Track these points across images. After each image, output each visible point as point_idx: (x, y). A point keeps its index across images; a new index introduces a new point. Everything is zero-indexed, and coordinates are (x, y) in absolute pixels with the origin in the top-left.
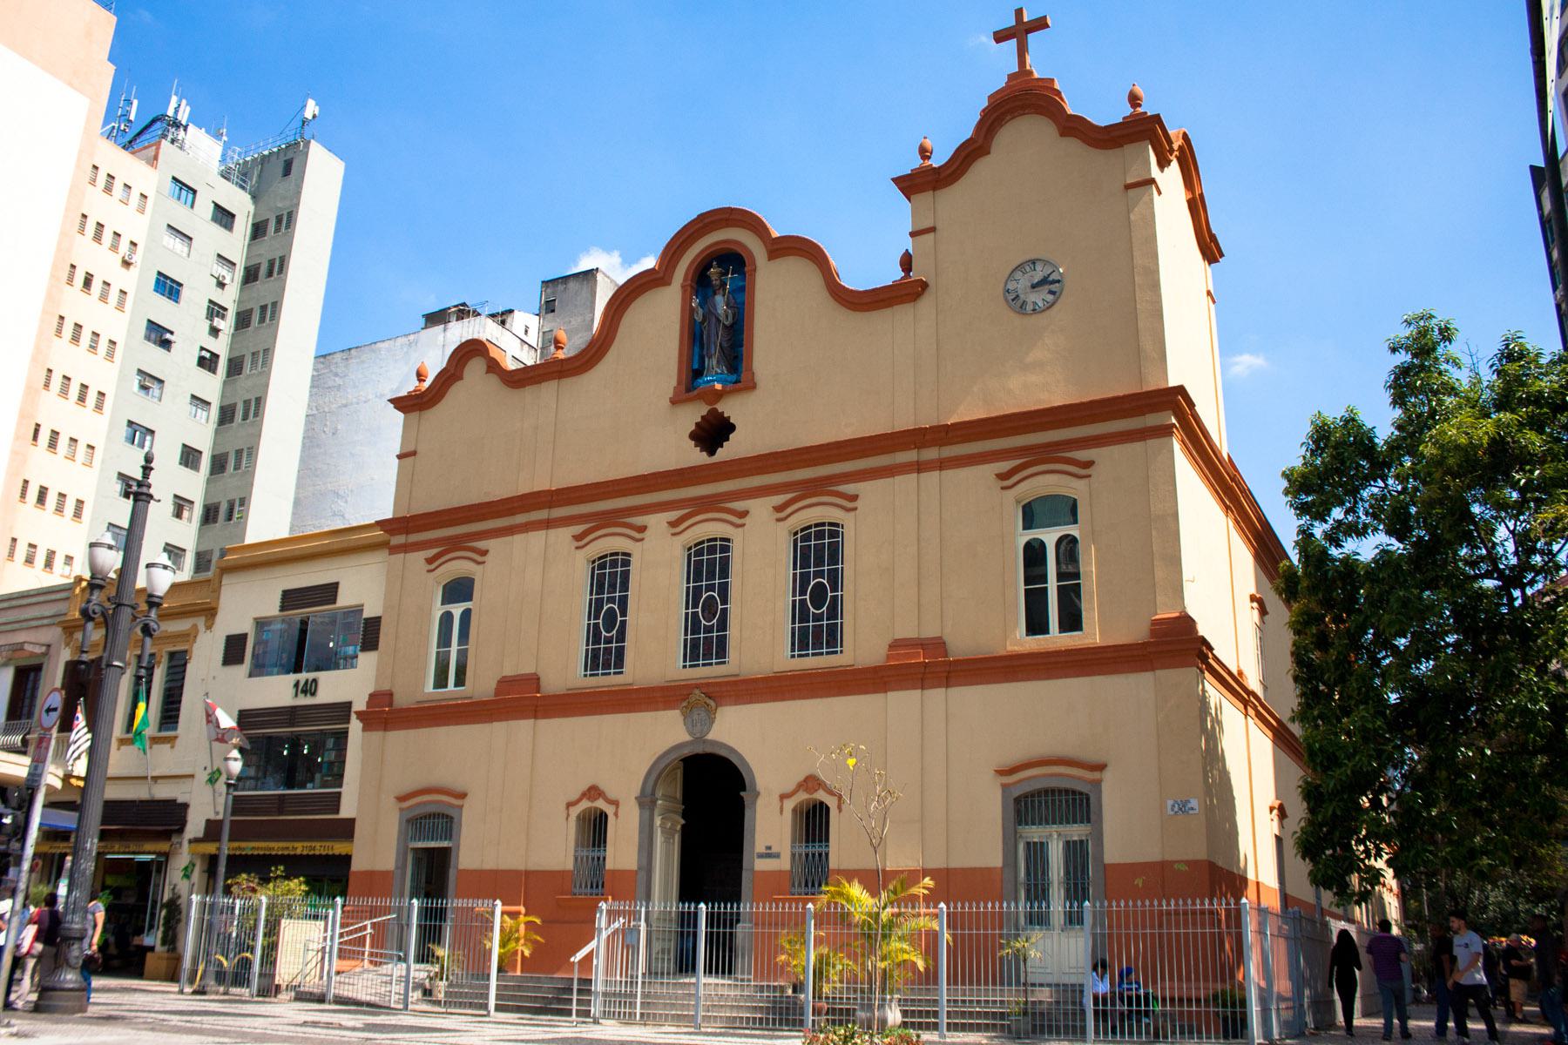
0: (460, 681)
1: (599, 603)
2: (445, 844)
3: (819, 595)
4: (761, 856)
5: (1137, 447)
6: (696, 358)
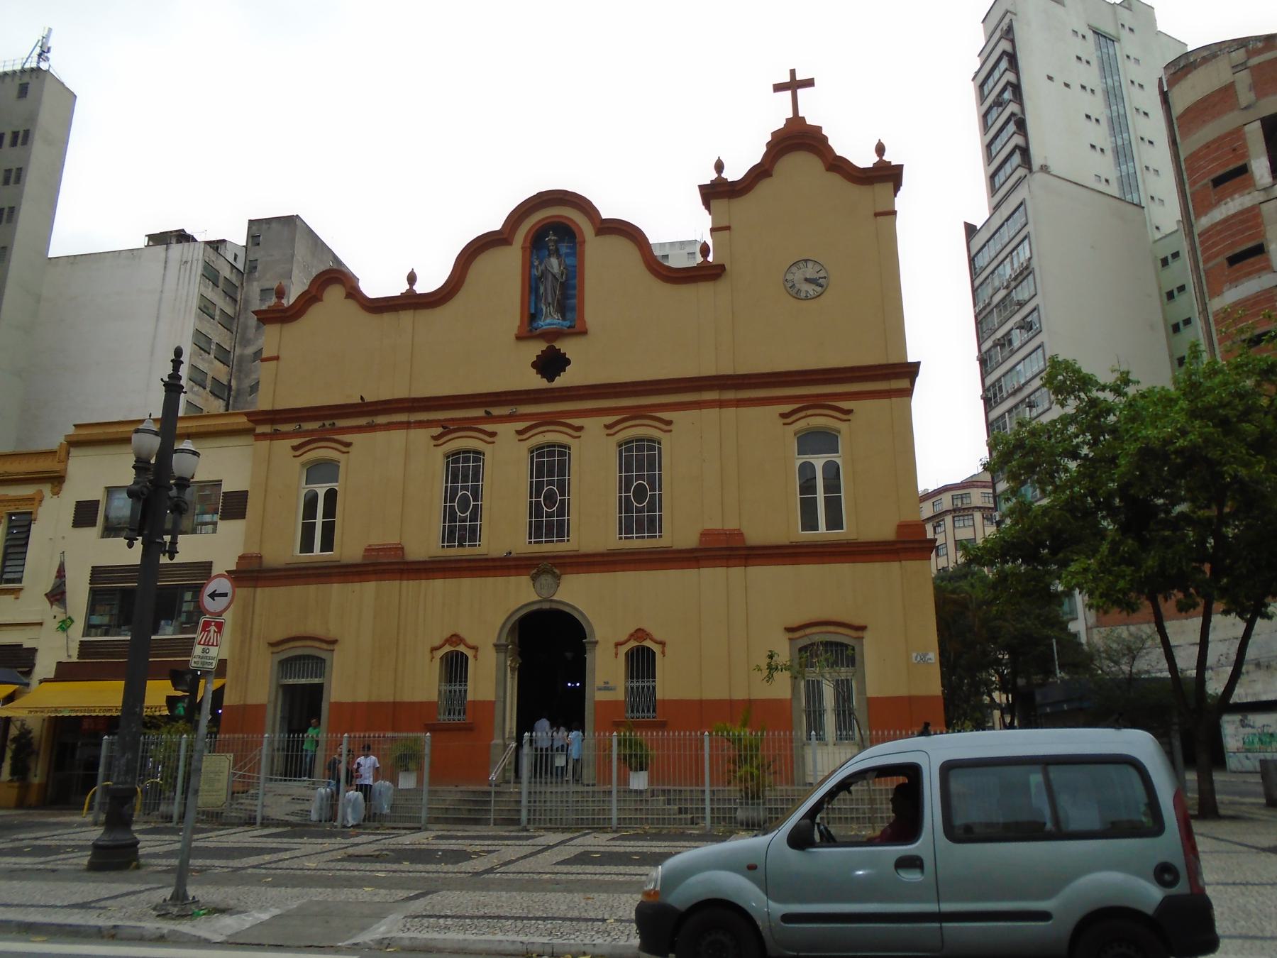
1: (454, 492)
2: (316, 681)
4: (600, 689)
5: (884, 402)
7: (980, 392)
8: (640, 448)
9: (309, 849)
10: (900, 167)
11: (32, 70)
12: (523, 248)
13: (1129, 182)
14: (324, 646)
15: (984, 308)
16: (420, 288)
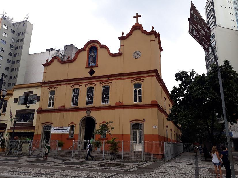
0: (52, 106)
3: (106, 96)
6: (89, 62)
8: (106, 87)
11: (25, 21)
12: (88, 51)
16: (70, 59)
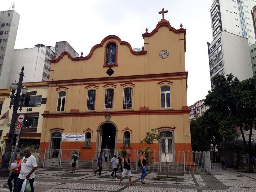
4: (118, 140)
5: (180, 80)
7: (210, 79)
8: (128, 90)
9: (50, 173)
10: (185, 29)
12: (105, 48)
13: (244, 33)
14: (61, 130)
15: (211, 61)
16: (84, 56)
